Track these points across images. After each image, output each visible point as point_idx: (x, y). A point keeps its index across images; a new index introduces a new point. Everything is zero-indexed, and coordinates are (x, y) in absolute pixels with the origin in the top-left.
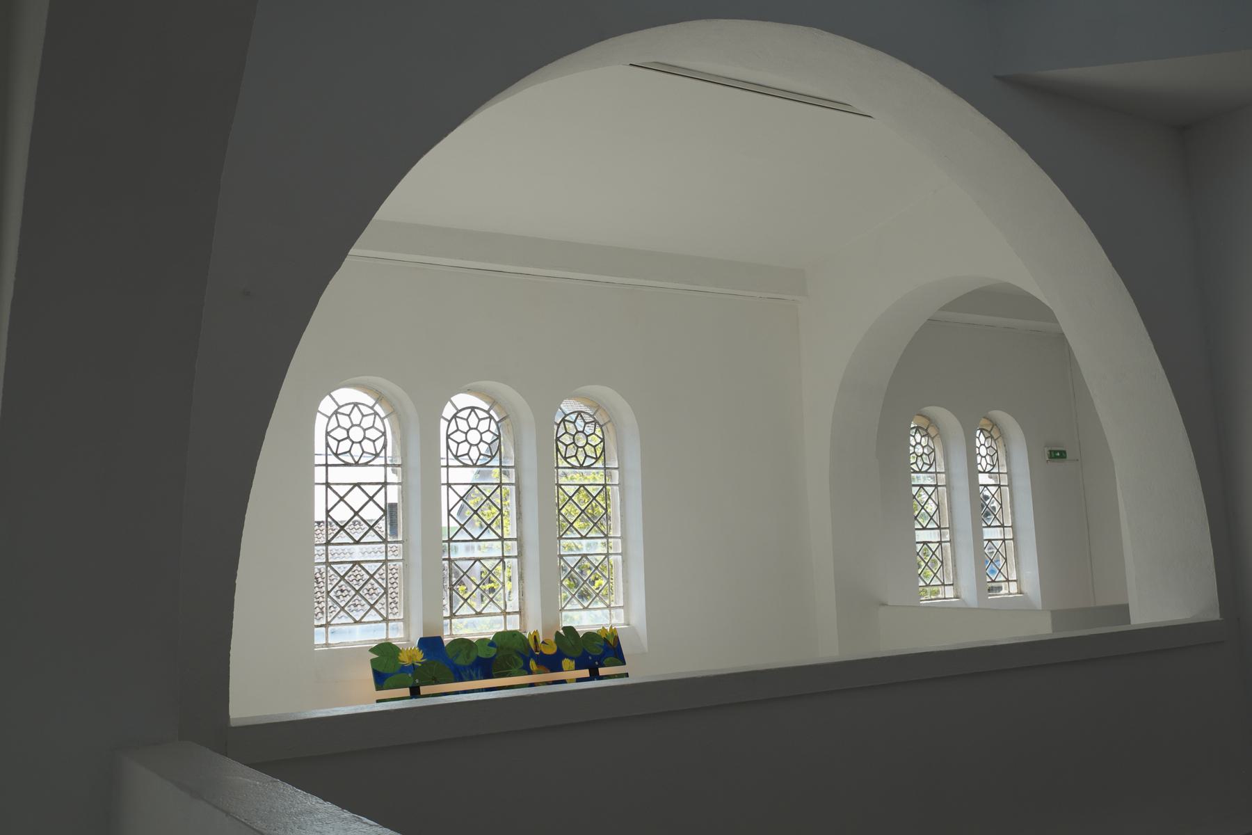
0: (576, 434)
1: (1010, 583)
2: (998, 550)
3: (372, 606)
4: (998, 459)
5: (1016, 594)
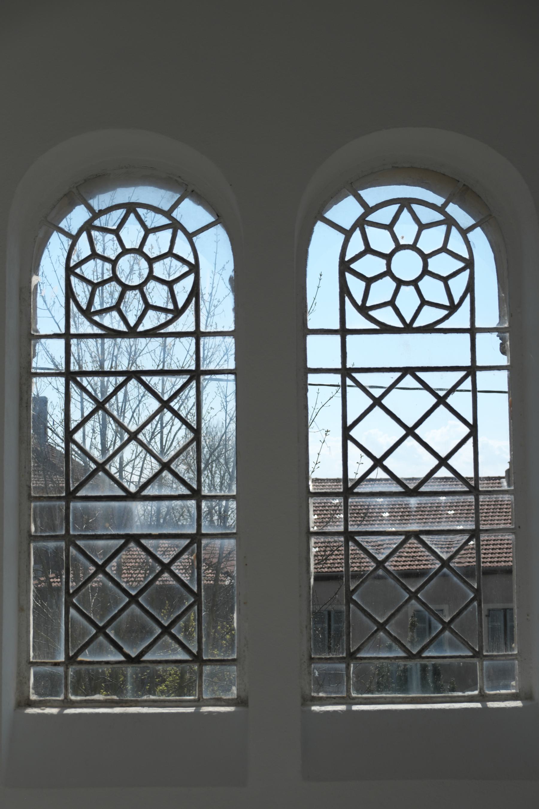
3: (166, 630)
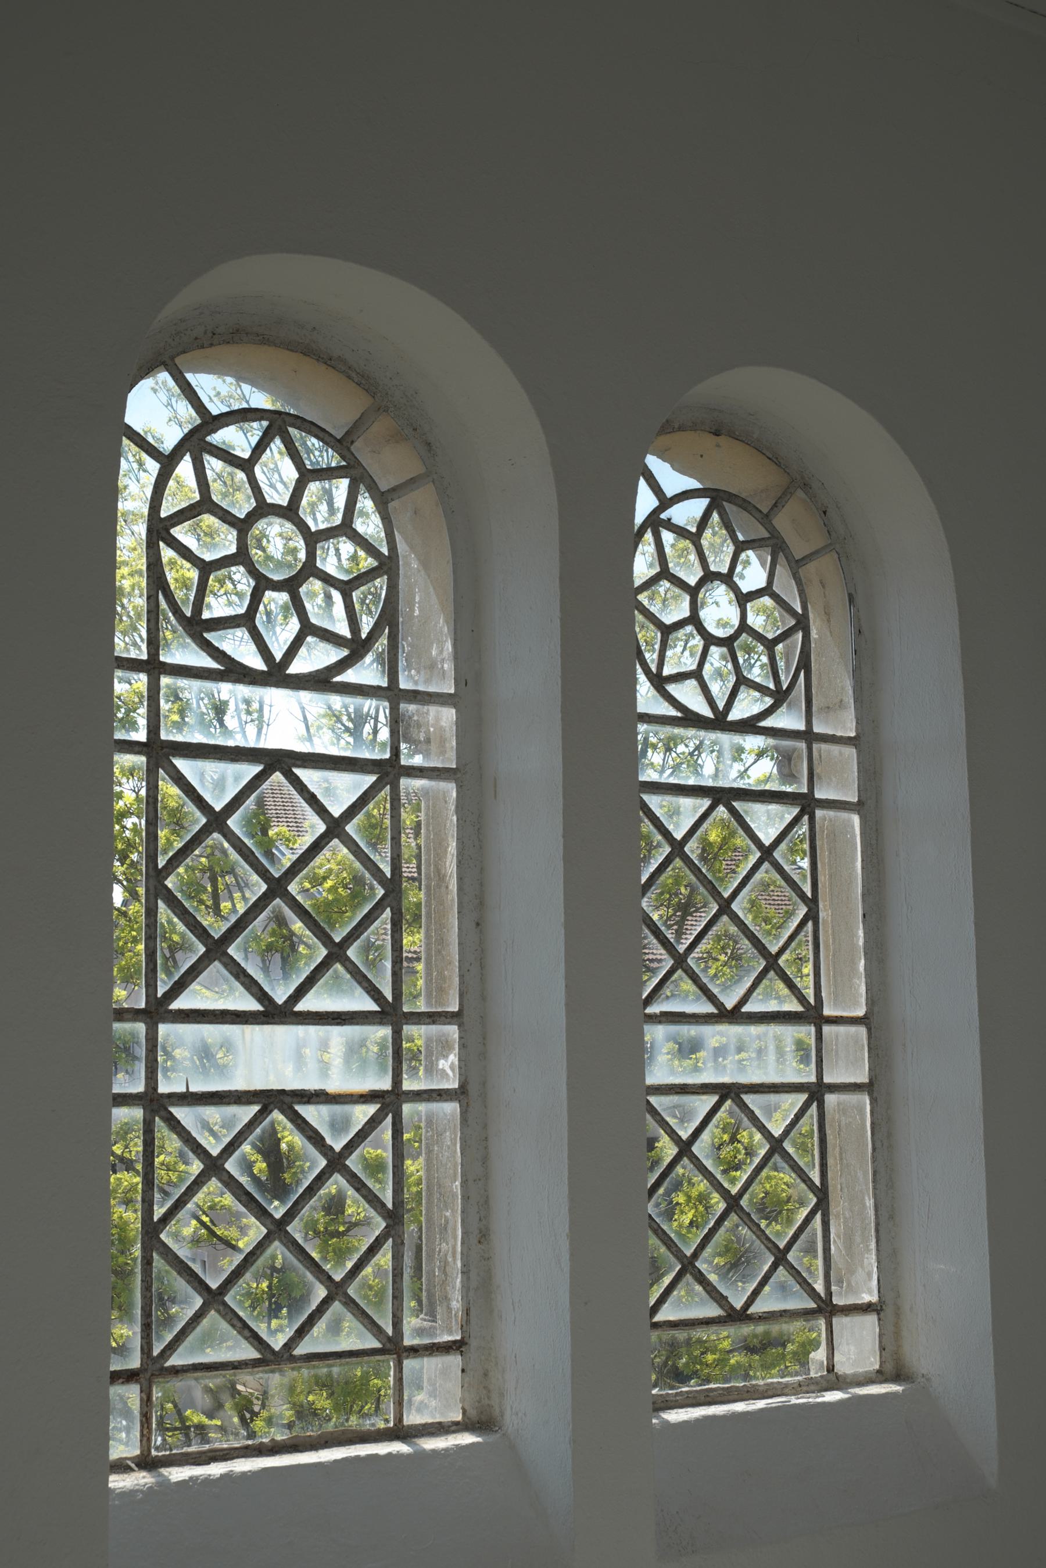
0: (701, 583)
1: (840, 1322)
2: (776, 1145)
4: (805, 664)
5: (869, 1380)
